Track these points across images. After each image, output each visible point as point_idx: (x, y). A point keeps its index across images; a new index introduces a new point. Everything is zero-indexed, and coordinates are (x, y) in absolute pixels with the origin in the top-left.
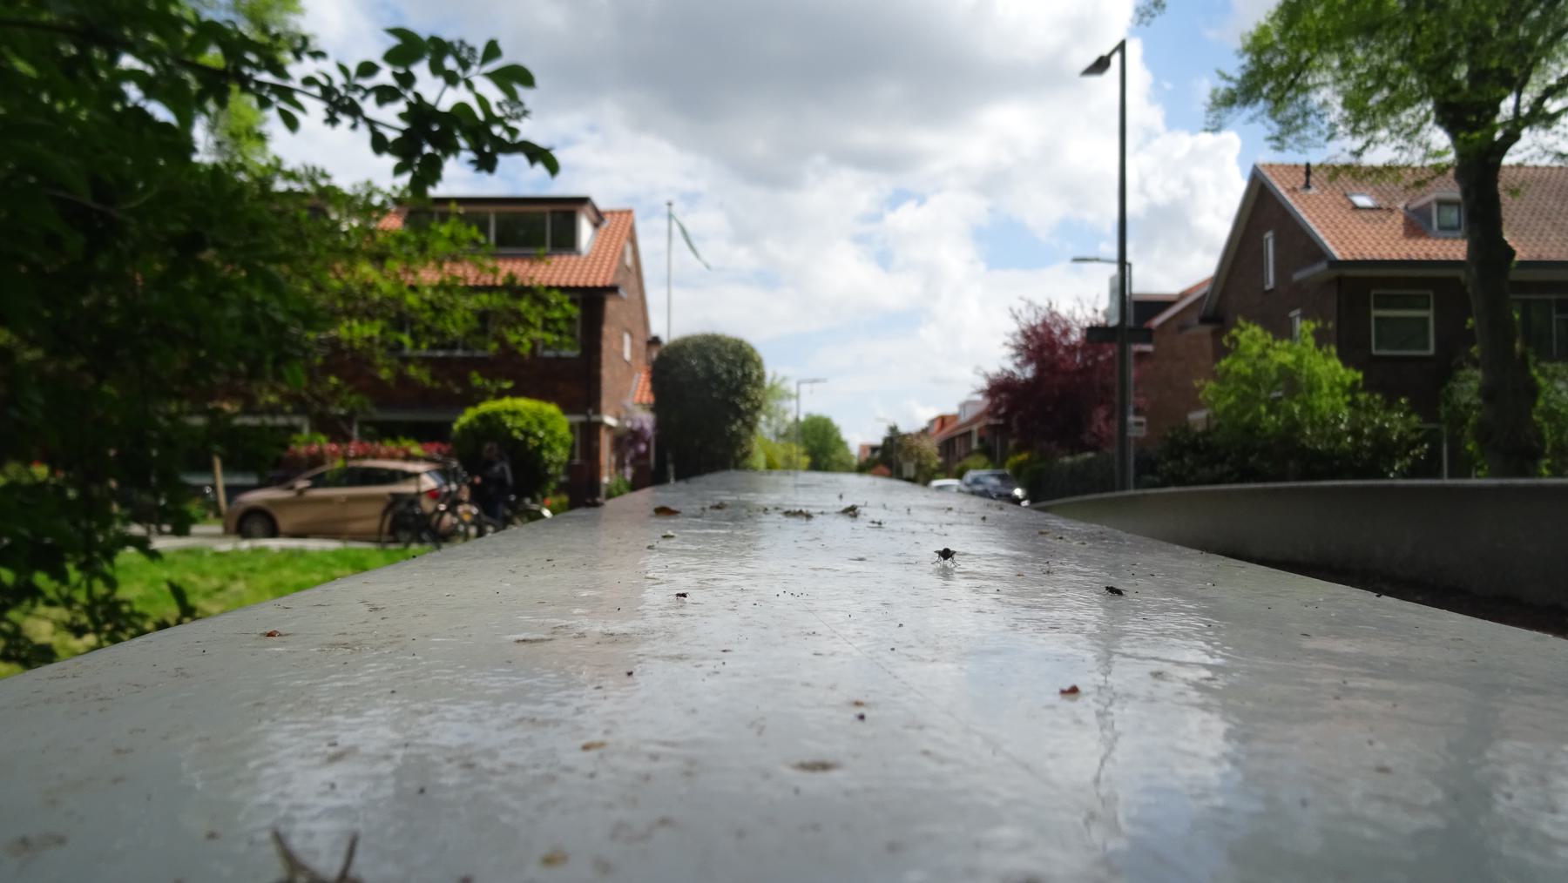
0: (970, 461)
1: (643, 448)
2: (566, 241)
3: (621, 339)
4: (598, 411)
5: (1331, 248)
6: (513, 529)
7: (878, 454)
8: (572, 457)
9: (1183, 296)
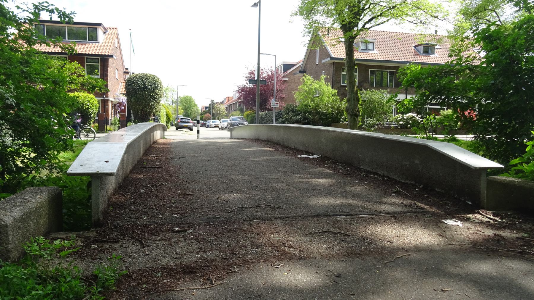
0: (234, 113)
1: (123, 108)
2: (94, 38)
3: (115, 71)
4: (107, 97)
5: (332, 54)
6: (196, 104)
8: (99, 111)
9: (298, 63)
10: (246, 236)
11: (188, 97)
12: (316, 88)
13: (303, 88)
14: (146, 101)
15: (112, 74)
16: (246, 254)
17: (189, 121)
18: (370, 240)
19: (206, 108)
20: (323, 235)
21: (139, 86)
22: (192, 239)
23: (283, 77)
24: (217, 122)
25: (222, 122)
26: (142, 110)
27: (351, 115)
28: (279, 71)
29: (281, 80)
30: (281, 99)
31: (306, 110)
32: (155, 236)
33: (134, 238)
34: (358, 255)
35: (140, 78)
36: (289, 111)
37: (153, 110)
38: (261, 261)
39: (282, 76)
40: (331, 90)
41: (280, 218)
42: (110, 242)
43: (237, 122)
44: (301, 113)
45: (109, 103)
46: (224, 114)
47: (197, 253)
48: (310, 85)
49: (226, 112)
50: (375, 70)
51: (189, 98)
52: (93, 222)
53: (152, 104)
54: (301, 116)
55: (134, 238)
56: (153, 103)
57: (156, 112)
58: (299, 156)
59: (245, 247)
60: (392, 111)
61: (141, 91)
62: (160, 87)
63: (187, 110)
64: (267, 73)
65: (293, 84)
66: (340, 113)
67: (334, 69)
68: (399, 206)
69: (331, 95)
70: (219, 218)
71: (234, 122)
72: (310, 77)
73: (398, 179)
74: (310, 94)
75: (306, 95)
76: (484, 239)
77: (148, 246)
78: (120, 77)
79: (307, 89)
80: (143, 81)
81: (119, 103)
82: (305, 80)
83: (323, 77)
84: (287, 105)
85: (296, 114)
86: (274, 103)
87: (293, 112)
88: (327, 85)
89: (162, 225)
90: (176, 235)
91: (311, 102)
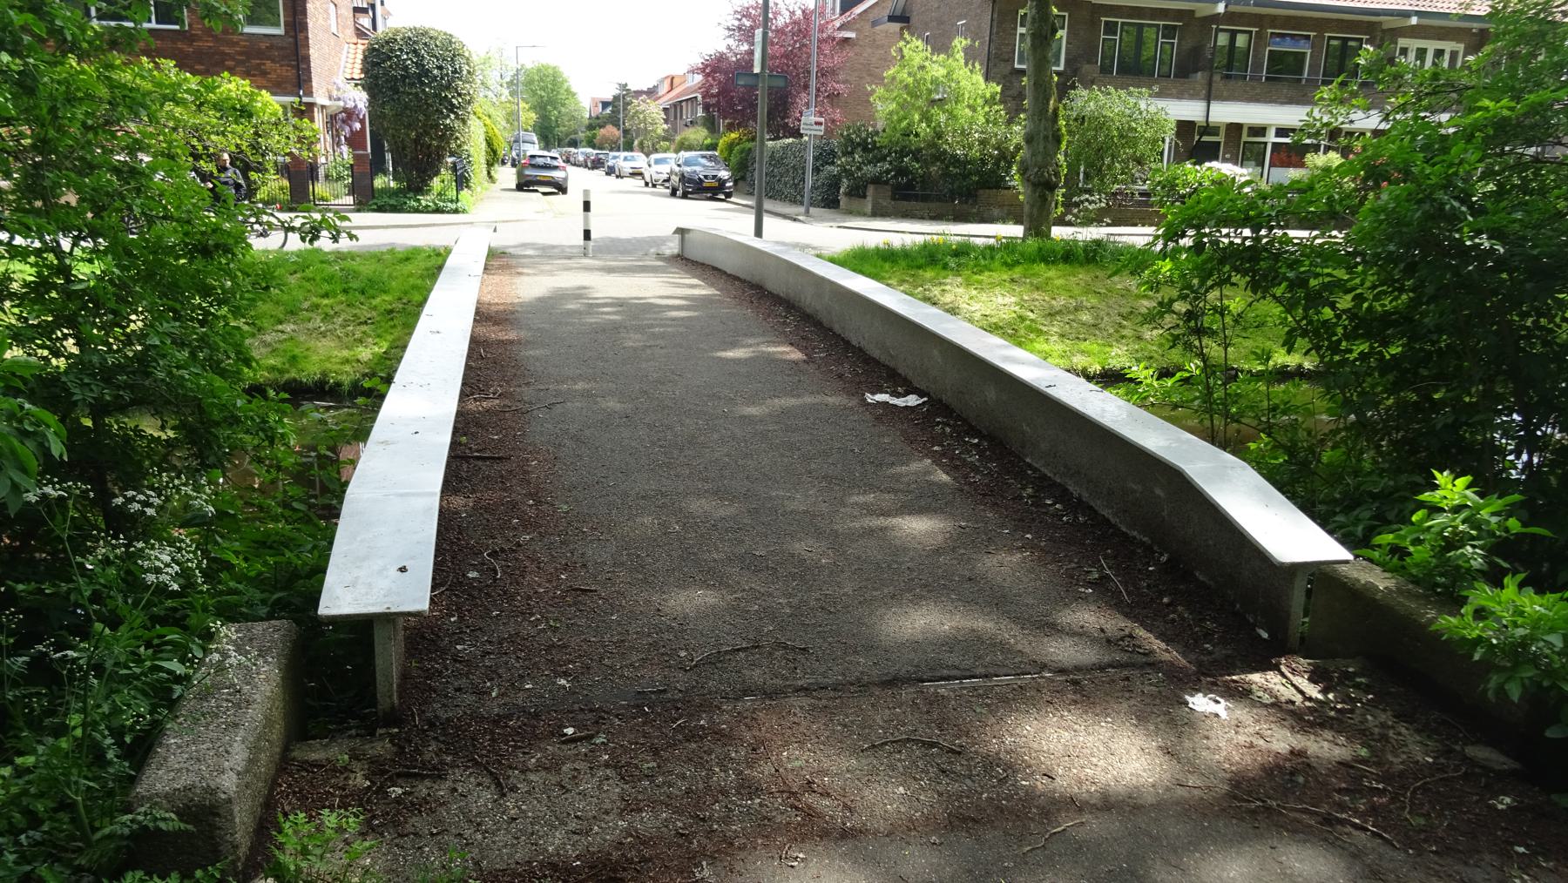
1: (358, 126)
3: (326, 11)
4: (310, 93)
6: (574, 89)
7: (608, 111)
10: (727, 756)
11: (547, 68)
12: (937, 78)
13: (899, 77)
14: (427, 117)
15: (321, 21)
16: (727, 820)
17: (555, 163)
18: (1004, 770)
19: (605, 104)
20: (900, 752)
21: (406, 68)
22: (607, 765)
23: (841, 28)
24: (639, 160)
25: (652, 163)
26: (416, 141)
27: (1035, 185)
28: (828, 10)
29: (834, 39)
30: (833, 97)
31: (905, 147)
32: (524, 753)
33: (477, 763)
34: (970, 825)
35: (406, 43)
36: (855, 146)
37: (448, 143)
38: (760, 841)
39: (837, 24)
40: (983, 86)
41: (806, 689)
42: (427, 776)
43: (698, 169)
44: (890, 153)
45: (316, 114)
46: (659, 131)
47: (621, 816)
48: (922, 68)
49: (665, 126)
50: (1120, 20)
51: (551, 71)
52: (381, 714)
53: (445, 126)
54: (891, 163)
55: (477, 763)
56: (448, 121)
57: (459, 146)
58: (870, 398)
59: (724, 792)
60: (1162, 154)
61: (412, 85)
62: (469, 72)
63: (545, 109)
64: (793, 13)
65: (869, 50)
66: (1005, 158)
67: (995, 16)
68: (1094, 640)
69: (980, 101)
70: (664, 691)
71: (688, 169)
72: (919, 43)
73: (1113, 520)
74: (917, 97)
75: (905, 100)
76: (1263, 768)
77: (511, 790)
78: (345, 27)
79: (910, 80)
80: (415, 51)
81: (345, 110)
82: (906, 51)
83: (960, 43)
84: (849, 128)
85: (874, 157)
86: (811, 122)
87: (865, 149)
88: (971, 71)
89: (536, 716)
90: (570, 751)
91: (921, 121)
